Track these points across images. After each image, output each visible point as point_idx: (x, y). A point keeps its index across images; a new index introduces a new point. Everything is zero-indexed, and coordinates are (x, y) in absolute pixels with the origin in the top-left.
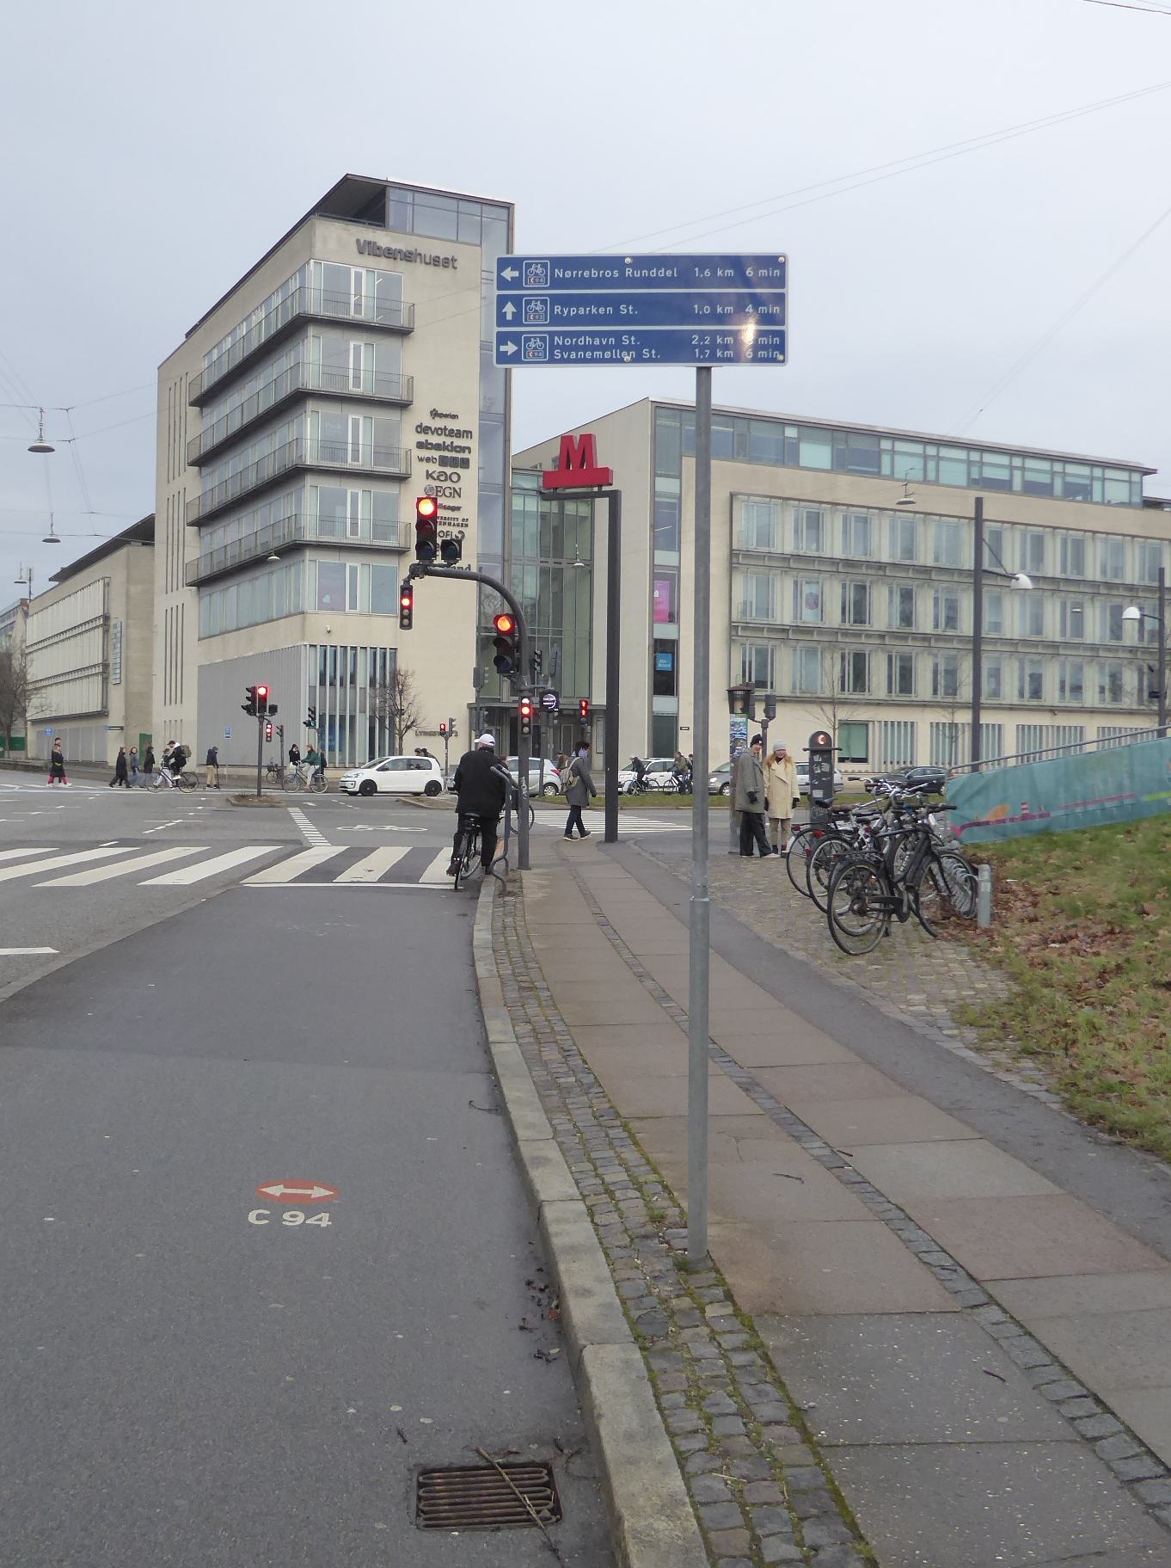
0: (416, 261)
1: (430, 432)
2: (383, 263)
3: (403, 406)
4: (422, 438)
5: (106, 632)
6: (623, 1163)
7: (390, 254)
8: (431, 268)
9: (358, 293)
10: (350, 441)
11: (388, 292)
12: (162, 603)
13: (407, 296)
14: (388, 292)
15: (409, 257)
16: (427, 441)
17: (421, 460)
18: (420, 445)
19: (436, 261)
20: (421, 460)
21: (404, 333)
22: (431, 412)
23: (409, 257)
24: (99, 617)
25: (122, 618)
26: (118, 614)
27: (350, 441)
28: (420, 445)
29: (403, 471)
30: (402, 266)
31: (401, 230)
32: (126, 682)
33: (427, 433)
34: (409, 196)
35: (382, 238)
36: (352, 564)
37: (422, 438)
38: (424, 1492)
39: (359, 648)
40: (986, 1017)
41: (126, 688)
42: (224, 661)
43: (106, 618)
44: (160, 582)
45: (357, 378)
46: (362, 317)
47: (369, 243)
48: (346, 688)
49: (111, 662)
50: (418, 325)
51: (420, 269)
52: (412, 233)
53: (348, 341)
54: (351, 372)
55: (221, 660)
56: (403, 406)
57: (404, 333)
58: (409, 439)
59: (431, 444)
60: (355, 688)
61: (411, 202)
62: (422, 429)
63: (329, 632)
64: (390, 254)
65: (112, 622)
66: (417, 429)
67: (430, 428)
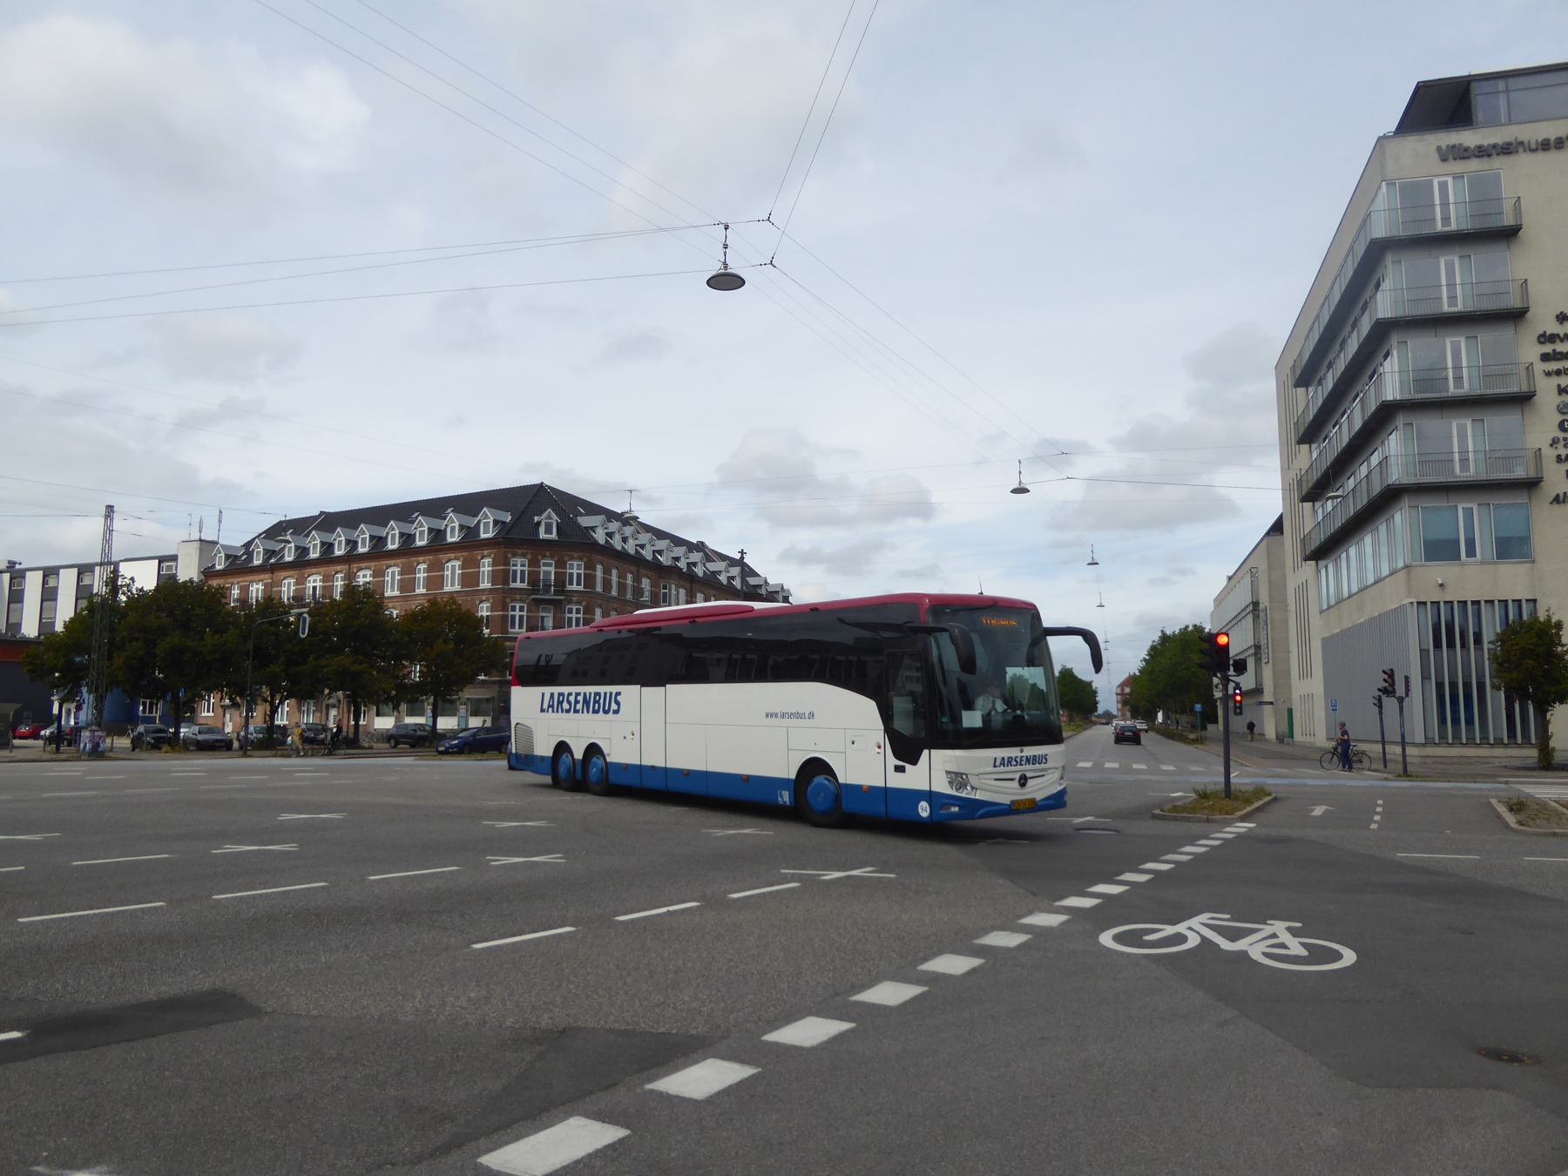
0: (1517, 152)
1: (1558, 341)
2: (1474, 165)
3: (1515, 316)
4: (1548, 348)
5: (1256, 618)
6: (66, 927)
7: (1482, 152)
8: (1541, 156)
9: (1445, 204)
10: (1450, 365)
11: (1485, 194)
12: (1293, 581)
13: (1508, 191)
14: (1485, 194)
15: (1507, 150)
16: (1554, 350)
17: (1548, 374)
18: (1545, 358)
19: (1545, 146)
20: (1548, 374)
21: (1509, 234)
22: (1557, 317)
23: (1507, 150)
24: (1249, 605)
25: (1267, 604)
26: (1264, 601)
27: (1450, 365)
28: (1545, 358)
29: (1525, 389)
30: (1497, 162)
31: (1494, 122)
32: (1273, 660)
33: (1554, 342)
34: (1501, 85)
35: (1468, 138)
36: (1466, 505)
37: (1548, 348)
38: (1338, 956)
39: (1483, 603)
40: (555, 963)
41: (1274, 666)
42: (1341, 631)
43: (1256, 604)
44: (1289, 562)
45: (1464, 461)
46: (1466, 389)
47: (1454, 146)
48: (1469, 650)
49: (1263, 642)
50: (1527, 222)
51: (1523, 160)
52: (1510, 123)
53: (1444, 340)
54: (1438, 209)
55: (1338, 630)
56: (1515, 316)
57: (1509, 234)
58: (1530, 352)
59: (1561, 353)
60: (1482, 649)
61: (1504, 89)
62: (1545, 338)
63: (1441, 585)
64: (1482, 152)
65: (1262, 606)
66: (1538, 338)
67: (1558, 335)
